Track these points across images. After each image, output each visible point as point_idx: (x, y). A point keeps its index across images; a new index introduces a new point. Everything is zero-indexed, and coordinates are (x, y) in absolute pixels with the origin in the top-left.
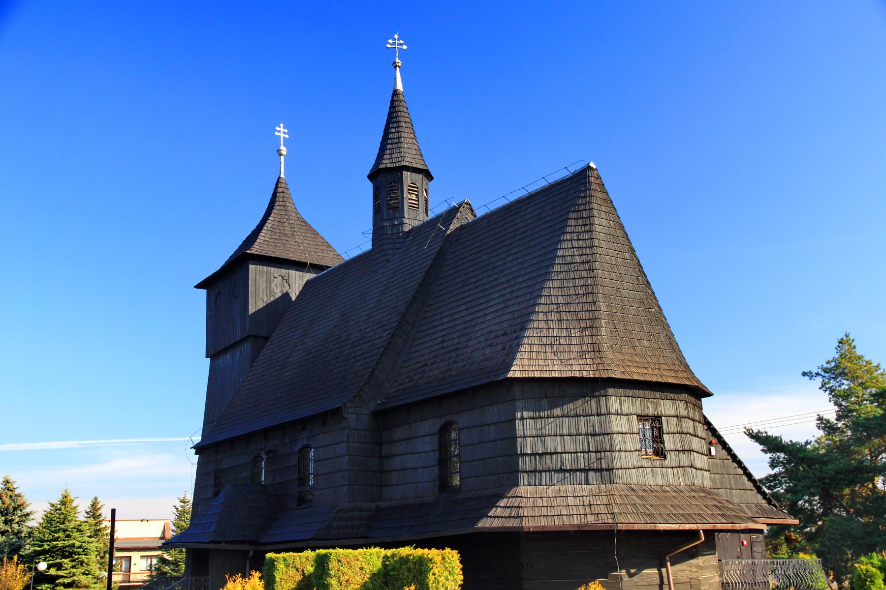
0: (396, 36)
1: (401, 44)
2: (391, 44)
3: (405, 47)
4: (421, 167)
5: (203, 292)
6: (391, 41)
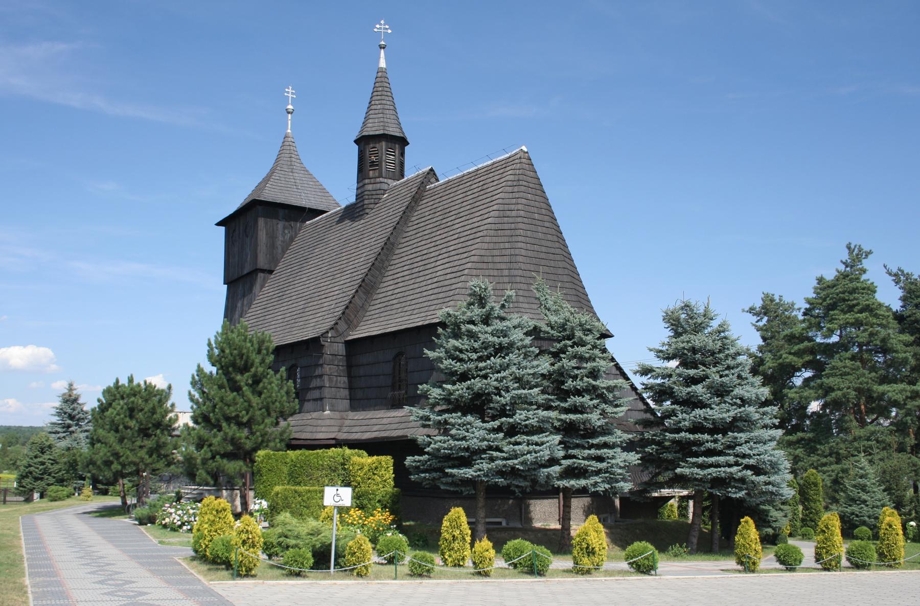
0: (382, 22)
1: (387, 29)
2: (378, 29)
3: (389, 31)
4: (398, 134)
5: (222, 229)
6: (378, 26)
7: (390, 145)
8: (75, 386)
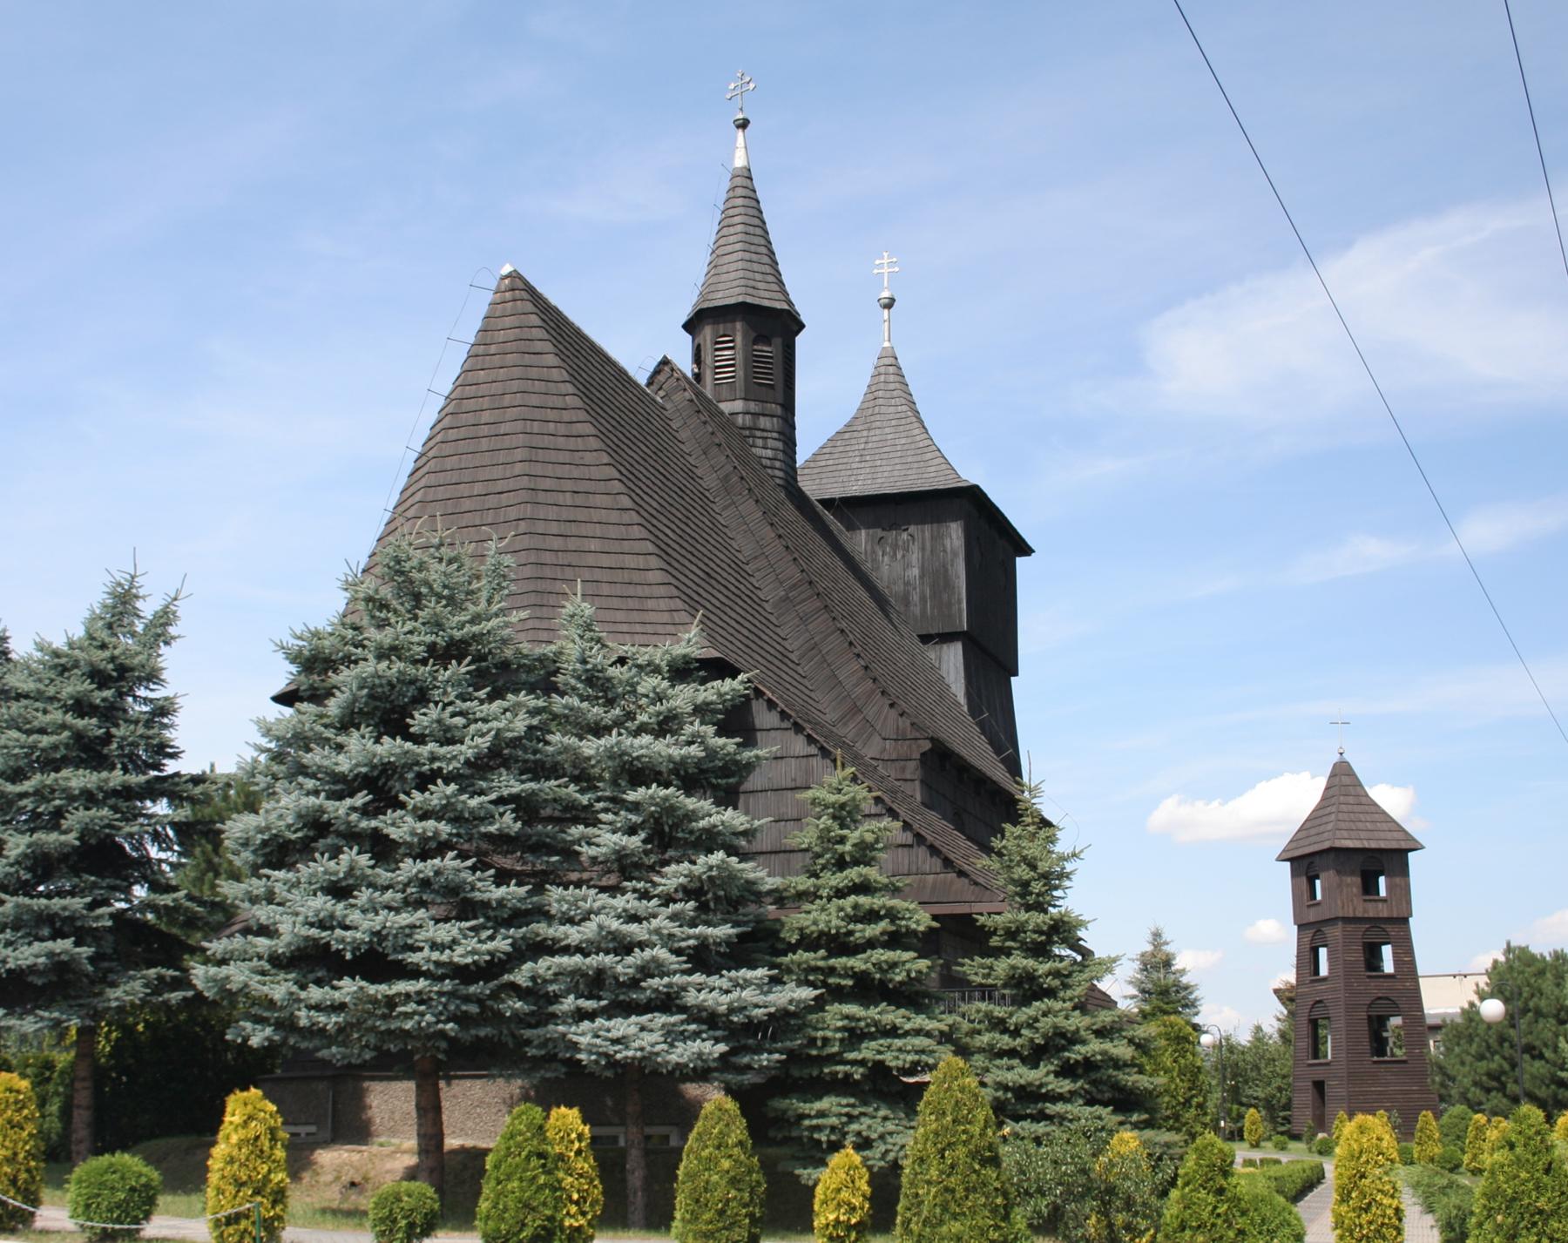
4: (778, 305)
7: (721, 328)
8: (1166, 937)
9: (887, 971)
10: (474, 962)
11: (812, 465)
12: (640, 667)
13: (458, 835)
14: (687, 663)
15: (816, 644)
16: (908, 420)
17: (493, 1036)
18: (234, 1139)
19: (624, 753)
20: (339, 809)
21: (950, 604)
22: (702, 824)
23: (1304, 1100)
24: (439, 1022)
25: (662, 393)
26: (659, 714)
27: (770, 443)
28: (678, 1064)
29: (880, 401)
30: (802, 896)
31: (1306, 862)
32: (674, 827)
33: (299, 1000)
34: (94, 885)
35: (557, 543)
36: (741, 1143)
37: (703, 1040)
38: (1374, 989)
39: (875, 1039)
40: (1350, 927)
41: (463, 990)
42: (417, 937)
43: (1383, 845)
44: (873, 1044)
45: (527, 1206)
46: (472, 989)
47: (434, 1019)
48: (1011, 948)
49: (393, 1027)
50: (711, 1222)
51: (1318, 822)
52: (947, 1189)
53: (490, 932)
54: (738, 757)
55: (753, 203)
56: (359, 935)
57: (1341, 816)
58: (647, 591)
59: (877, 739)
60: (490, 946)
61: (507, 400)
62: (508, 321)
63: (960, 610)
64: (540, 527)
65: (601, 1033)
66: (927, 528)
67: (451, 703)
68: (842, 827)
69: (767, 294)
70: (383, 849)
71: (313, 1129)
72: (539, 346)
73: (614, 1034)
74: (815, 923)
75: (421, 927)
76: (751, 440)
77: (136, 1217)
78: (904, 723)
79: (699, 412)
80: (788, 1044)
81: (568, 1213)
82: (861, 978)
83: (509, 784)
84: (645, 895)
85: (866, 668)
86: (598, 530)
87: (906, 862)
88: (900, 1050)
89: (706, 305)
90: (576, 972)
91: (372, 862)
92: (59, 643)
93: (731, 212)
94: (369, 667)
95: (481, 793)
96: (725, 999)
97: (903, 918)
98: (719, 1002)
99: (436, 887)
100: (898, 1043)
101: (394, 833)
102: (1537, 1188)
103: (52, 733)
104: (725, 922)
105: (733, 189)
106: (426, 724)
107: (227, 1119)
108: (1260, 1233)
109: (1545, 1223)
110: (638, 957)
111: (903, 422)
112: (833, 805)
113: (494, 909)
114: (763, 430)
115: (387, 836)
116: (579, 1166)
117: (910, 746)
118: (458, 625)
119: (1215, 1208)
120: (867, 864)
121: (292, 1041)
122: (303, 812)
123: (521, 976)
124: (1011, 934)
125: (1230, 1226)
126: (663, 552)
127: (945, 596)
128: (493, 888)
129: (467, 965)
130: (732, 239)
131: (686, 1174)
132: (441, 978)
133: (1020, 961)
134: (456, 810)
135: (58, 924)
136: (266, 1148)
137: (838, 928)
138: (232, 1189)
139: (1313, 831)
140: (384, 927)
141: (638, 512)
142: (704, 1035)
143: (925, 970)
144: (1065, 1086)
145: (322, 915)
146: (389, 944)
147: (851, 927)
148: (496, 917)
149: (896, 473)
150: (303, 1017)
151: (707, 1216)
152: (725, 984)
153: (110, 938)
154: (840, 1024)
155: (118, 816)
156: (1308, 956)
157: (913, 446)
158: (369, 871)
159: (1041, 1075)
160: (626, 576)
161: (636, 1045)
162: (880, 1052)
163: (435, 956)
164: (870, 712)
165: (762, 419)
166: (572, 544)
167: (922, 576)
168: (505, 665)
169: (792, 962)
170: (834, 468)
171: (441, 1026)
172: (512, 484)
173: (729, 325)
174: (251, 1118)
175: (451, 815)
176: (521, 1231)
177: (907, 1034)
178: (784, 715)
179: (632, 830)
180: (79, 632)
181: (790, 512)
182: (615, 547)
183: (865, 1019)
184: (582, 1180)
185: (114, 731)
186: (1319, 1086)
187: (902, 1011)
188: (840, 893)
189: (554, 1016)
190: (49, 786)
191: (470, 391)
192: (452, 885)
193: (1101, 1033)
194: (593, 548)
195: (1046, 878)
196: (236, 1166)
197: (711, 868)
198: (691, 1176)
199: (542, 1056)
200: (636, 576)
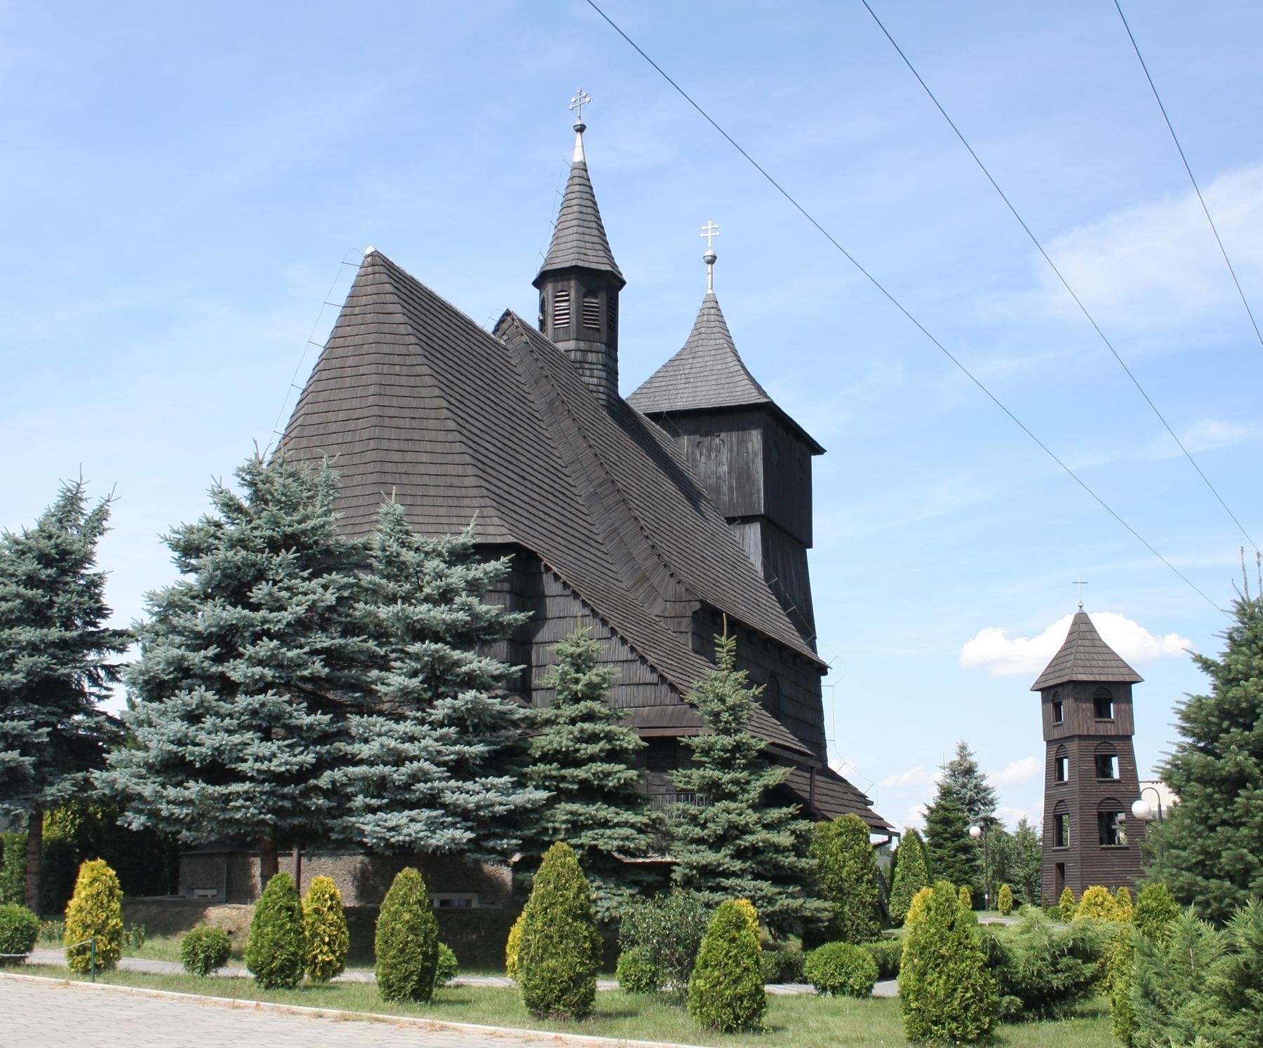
4: (603, 268)
8: (970, 749)
9: (603, 779)
10: (287, 770)
11: (649, 385)
12: (427, 553)
13: (280, 677)
14: (466, 549)
15: (616, 529)
16: (724, 351)
17: (306, 824)
18: (83, 894)
19: (407, 617)
20: (195, 658)
21: (751, 494)
22: (464, 669)
23: (1050, 876)
24: (261, 813)
25: (505, 337)
26: (439, 587)
27: (596, 373)
28: (438, 847)
29: (703, 336)
30: (549, 722)
31: (1052, 693)
32: (443, 672)
33: (162, 797)
34: (38, 712)
35: (397, 457)
36: (419, 902)
37: (457, 829)
38: (1104, 791)
39: (593, 829)
40: (1084, 743)
41: (280, 791)
42: (245, 751)
43: (1111, 678)
44: (590, 833)
45: (276, 944)
46: (286, 790)
47: (256, 811)
48: (706, 762)
49: (227, 817)
50: (394, 957)
51: (1061, 660)
52: (547, 936)
53: (302, 748)
54: (501, 619)
55: (588, 189)
56: (204, 750)
57: (1078, 656)
58: (463, 492)
59: (660, 601)
60: (300, 758)
61: (365, 349)
62: (369, 289)
63: (759, 498)
64: (385, 445)
65: (380, 823)
66: (734, 434)
67: (281, 581)
68: (577, 671)
69: (595, 259)
70: (227, 688)
71: (214, 892)
72: (391, 308)
73: (390, 824)
74: (551, 743)
75: (248, 744)
76: (581, 371)
77: (19, 949)
78: (681, 589)
79: (532, 351)
80: (526, 832)
81: (321, 951)
82: (584, 783)
83: (322, 640)
84: (422, 722)
85: (653, 547)
86: (428, 446)
87: (653, 697)
88: (610, 837)
89: (548, 268)
90: (364, 778)
91: (217, 697)
92: (19, 535)
93: (570, 196)
94: (222, 554)
95: (301, 647)
96: (475, 798)
97: (618, 740)
98: (460, 798)
99: (262, 715)
100: (608, 832)
101: (235, 676)
102: (941, 939)
103: (10, 600)
104: (480, 742)
105: (572, 178)
106: (260, 596)
107: (80, 880)
108: (840, 974)
109: (946, 964)
110: (408, 768)
111: (720, 352)
112: (572, 655)
113: (306, 731)
114: (590, 363)
115: (229, 678)
116: (330, 917)
117: (684, 607)
118: (290, 523)
119: (729, 952)
120: (593, 699)
121: (161, 826)
122: (170, 660)
123: (324, 780)
124: (706, 752)
125: (738, 965)
126: (480, 463)
127: (747, 488)
128: (304, 716)
129: (282, 773)
130: (570, 217)
131: (381, 924)
132: (263, 782)
133: (712, 773)
134: (277, 659)
135: (10, 740)
136: (105, 902)
137: (567, 747)
138: (80, 930)
139: (1058, 668)
140: (221, 745)
141: (460, 433)
142: (458, 825)
143: (635, 778)
144: (738, 865)
145: (179, 735)
146: (226, 756)
147: (578, 746)
148: (308, 737)
149: (712, 392)
150: (165, 809)
151: (391, 954)
152: (477, 787)
153: (51, 750)
154: (565, 818)
155: (54, 661)
156: (1054, 765)
157: (726, 371)
158: (214, 704)
159: (721, 858)
160: (448, 481)
161: (405, 831)
162: (594, 839)
163: (258, 765)
164: (655, 580)
165: (590, 355)
166: (409, 457)
167: (730, 473)
168: (328, 552)
169: (533, 772)
170: (665, 388)
171: (262, 816)
172: (365, 412)
173: (566, 283)
174: (95, 880)
175: (275, 663)
176: (272, 962)
177: (618, 825)
178: (566, 585)
179: (414, 674)
180: (33, 527)
181: (609, 425)
182: (440, 459)
183: (585, 814)
184: (333, 928)
185: (55, 598)
186: (1061, 867)
187: (613, 809)
188: (573, 721)
189: (350, 810)
190: (6, 639)
191: (340, 342)
192: (274, 714)
193: (767, 827)
194: (424, 460)
195: (733, 710)
196: (84, 914)
197: (467, 703)
198: (385, 924)
199: (343, 839)
200: (456, 482)
